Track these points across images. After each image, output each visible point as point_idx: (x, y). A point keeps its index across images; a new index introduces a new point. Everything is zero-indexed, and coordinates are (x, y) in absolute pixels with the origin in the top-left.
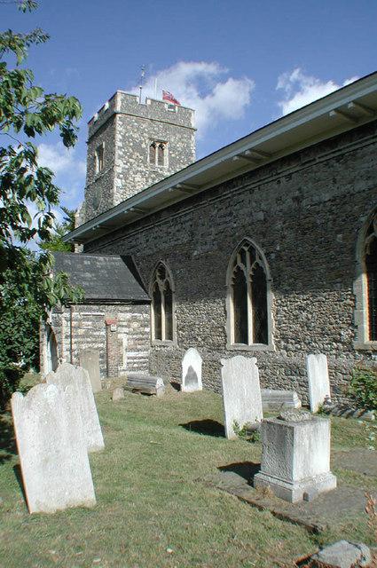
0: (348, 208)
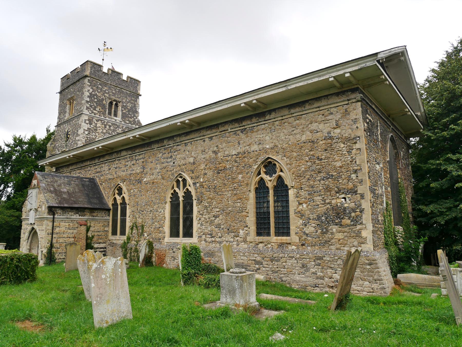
0: (246, 160)
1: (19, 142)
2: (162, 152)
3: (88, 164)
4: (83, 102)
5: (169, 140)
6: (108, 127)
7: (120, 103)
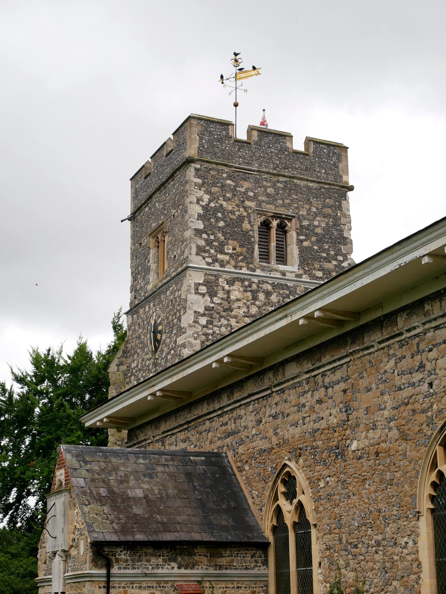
1: (46, 366)
2: (394, 355)
3: (205, 411)
4: (188, 234)
5: (410, 315)
6: (261, 296)
7: (290, 220)
